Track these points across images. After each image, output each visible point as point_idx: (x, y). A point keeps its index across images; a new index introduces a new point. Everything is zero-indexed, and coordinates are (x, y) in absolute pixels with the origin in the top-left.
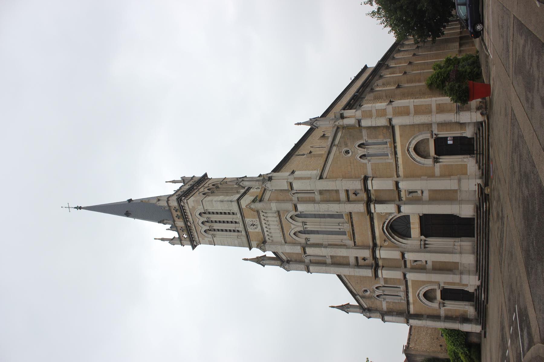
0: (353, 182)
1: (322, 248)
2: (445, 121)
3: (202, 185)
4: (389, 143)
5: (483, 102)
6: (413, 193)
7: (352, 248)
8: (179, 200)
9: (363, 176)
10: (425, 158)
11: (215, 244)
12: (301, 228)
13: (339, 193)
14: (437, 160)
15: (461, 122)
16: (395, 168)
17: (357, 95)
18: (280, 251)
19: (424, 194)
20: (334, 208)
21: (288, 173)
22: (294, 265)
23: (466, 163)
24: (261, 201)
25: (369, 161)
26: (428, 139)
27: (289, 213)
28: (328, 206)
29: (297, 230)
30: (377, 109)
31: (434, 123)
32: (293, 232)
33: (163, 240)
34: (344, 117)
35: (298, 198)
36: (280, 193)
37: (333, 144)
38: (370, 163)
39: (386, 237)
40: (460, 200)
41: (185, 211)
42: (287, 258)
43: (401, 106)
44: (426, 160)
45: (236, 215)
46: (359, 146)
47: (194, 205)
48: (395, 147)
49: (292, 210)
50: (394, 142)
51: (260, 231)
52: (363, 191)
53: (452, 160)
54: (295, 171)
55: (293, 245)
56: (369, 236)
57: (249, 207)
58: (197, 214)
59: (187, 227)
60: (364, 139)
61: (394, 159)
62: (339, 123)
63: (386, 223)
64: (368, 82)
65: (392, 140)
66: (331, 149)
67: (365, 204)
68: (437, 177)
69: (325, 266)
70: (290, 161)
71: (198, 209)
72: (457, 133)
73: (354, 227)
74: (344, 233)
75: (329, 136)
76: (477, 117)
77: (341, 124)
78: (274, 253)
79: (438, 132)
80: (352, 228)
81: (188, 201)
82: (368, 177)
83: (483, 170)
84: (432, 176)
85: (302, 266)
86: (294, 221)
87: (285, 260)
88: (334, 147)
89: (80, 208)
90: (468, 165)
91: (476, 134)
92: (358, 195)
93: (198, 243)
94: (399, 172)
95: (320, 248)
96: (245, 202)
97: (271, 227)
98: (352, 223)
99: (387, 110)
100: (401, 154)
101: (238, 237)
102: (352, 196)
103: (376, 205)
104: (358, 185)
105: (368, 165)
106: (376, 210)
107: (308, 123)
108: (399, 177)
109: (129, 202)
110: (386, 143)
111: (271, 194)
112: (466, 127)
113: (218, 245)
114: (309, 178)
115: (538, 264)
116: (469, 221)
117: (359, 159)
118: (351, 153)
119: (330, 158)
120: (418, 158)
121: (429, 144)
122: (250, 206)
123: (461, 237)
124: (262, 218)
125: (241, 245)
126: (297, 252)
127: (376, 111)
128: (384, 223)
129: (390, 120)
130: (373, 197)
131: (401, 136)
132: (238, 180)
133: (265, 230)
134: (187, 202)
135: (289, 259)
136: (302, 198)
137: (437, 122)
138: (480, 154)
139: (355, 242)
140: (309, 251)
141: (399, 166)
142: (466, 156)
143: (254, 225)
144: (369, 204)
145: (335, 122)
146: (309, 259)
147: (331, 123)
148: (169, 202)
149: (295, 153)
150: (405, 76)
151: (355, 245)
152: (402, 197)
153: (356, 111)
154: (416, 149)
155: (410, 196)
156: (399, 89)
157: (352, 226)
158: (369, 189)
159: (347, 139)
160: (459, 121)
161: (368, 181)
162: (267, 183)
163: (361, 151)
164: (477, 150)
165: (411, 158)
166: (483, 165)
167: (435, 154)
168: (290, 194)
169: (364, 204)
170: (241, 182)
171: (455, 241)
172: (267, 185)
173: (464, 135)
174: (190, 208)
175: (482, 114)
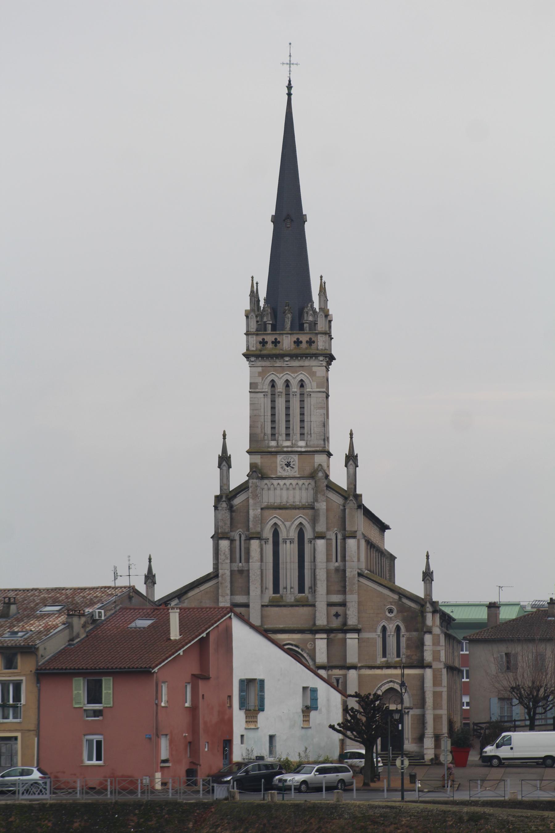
0: (355, 616)
2: (426, 723)
4: (399, 660)
12: (286, 535)
20: (321, 588)
25: (379, 636)
27: (308, 523)
28: (324, 580)
32: (279, 523)
37: (402, 596)
38: (377, 636)
42: (236, 505)
45: (299, 439)
51: (279, 474)
62: (428, 607)
63: (297, 649)
71: (311, 380)
73: (290, 608)
76: (429, 754)
80: (288, 605)
89: (289, 95)
92: (334, 618)
94: (364, 670)
102: (334, 610)
103: (326, 641)
110: (398, 655)
111: (336, 502)
117: (382, 625)
118: (389, 615)
122: (320, 470)
124: (301, 482)
128: (296, 646)
129: (430, 667)
130: (332, 635)
133: (282, 482)
136: (331, 544)
139: (267, 606)
152: (332, 671)
157: (292, 606)
162: (355, 503)
165: (381, 684)
172: (351, 502)
173: (406, 742)
174: (313, 368)
175: (432, 760)
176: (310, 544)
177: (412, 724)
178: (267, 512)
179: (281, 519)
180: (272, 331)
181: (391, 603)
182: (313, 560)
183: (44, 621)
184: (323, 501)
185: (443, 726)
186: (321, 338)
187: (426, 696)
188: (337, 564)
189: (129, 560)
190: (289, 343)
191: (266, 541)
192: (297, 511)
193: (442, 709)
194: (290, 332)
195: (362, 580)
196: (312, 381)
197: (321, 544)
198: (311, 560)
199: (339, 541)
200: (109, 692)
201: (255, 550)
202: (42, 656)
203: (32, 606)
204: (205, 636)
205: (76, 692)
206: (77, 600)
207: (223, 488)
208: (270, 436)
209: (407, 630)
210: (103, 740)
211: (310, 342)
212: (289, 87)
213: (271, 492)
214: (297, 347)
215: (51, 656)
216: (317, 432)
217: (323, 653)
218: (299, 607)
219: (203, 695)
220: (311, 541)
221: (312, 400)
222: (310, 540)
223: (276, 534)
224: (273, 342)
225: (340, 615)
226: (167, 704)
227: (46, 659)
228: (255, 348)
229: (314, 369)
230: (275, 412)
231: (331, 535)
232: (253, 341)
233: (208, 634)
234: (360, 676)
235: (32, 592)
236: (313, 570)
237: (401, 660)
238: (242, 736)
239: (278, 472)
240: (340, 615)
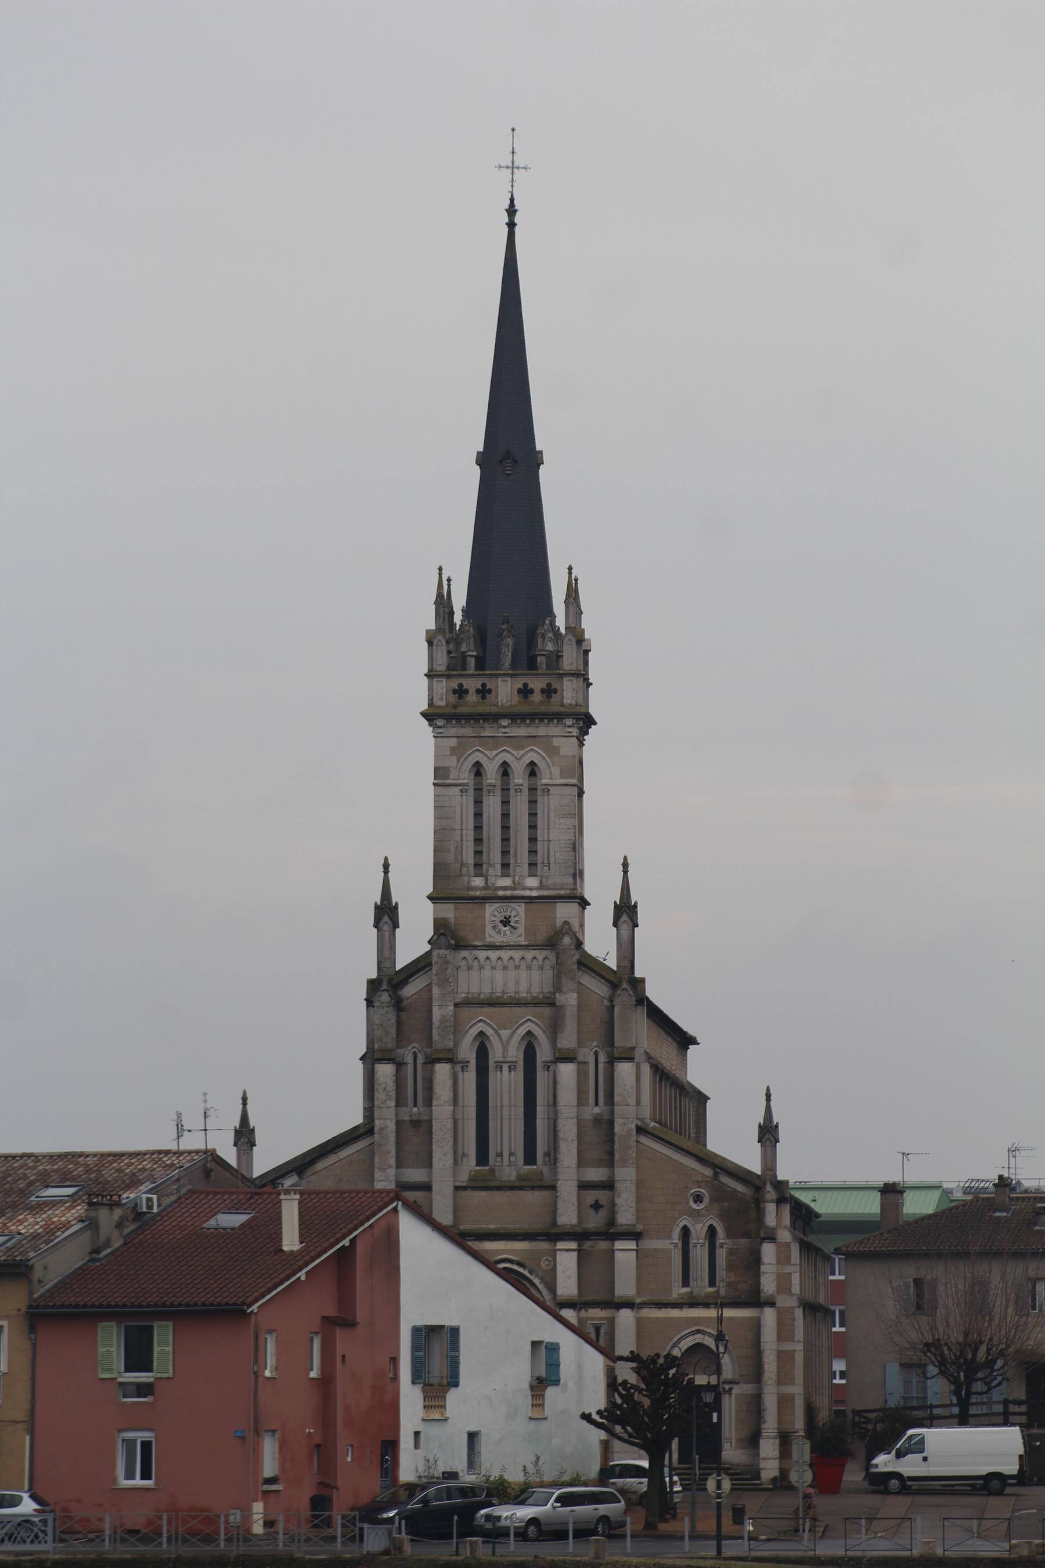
0: (631, 1207)
2: (764, 1410)
11: (437, 787)
12: (501, 1056)
13: (597, 1167)
27: (544, 1032)
28: (573, 1141)
31: (397, 1114)
32: (489, 1032)
38: (672, 1247)
42: (407, 998)
45: (527, 875)
49: (559, 1045)
62: (769, 1192)
63: (521, 1270)
73: (509, 1193)
75: (904, 1282)
89: (511, 225)
92: (592, 1211)
94: (648, 1309)
102: (591, 1196)
103: (575, 1254)
105: (667, 1242)
106: (564, 1252)
110: (712, 1283)
112: (743, 1449)
115: (980, 1377)
117: (681, 1225)
118: (695, 1206)
122: (566, 933)
124: (529, 955)
127: (787, 1273)
129: (772, 1304)
130: (587, 1245)
133: (493, 955)
135: (406, 1002)
139: (465, 1188)
147: (768, 1172)
152: (587, 1311)
157: (511, 1188)
162: (632, 994)
163: (698, 1230)
165: (679, 1336)
173: (726, 1446)
174: (554, 739)
175: (774, 1480)
176: (546, 1072)
177: (737, 1412)
178: (465, 1012)
179: (491, 1023)
180: (476, 669)
181: (699, 1184)
182: (551, 1102)
183: (44, 1216)
184: (572, 991)
185: (796, 1415)
189: (205, 1101)
191: (464, 1066)
193: (793, 1384)
194: (511, 672)
195: (644, 1140)
196: (551, 765)
197: (567, 1071)
198: (548, 1101)
199: (601, 1066)
200: (166, 1349)
201: (444, 1082)
202: (40, 1282)
203: (21, 1186)
204: (347, 1244)
205: (104, 1349)
206: (106, 1176)
209: (730, 1235)
210: (153, 1440)
211: (549, 691)
212: (512, 211)
214: (523, 700)
215: (55, 1281)
216: (560, 861)
217: (570, 1277)
219: (344, 1356)
220: (549, 1067)
221: (551, 801)
222: (547, 1064)
224: (478, 691)
225: (602, 1206)
226: (275, 1373)
227: (47, 1287)
229: (556, 742)
230: (482, 823)
231: (586, 1055)
232: (442, 689)
233: (353, 1241)
235: (21, 1161)
236: (552, 1121)
237: (718, 1292)
238: (417, 1434)
239: (487, 935)
240: (602, 1206)
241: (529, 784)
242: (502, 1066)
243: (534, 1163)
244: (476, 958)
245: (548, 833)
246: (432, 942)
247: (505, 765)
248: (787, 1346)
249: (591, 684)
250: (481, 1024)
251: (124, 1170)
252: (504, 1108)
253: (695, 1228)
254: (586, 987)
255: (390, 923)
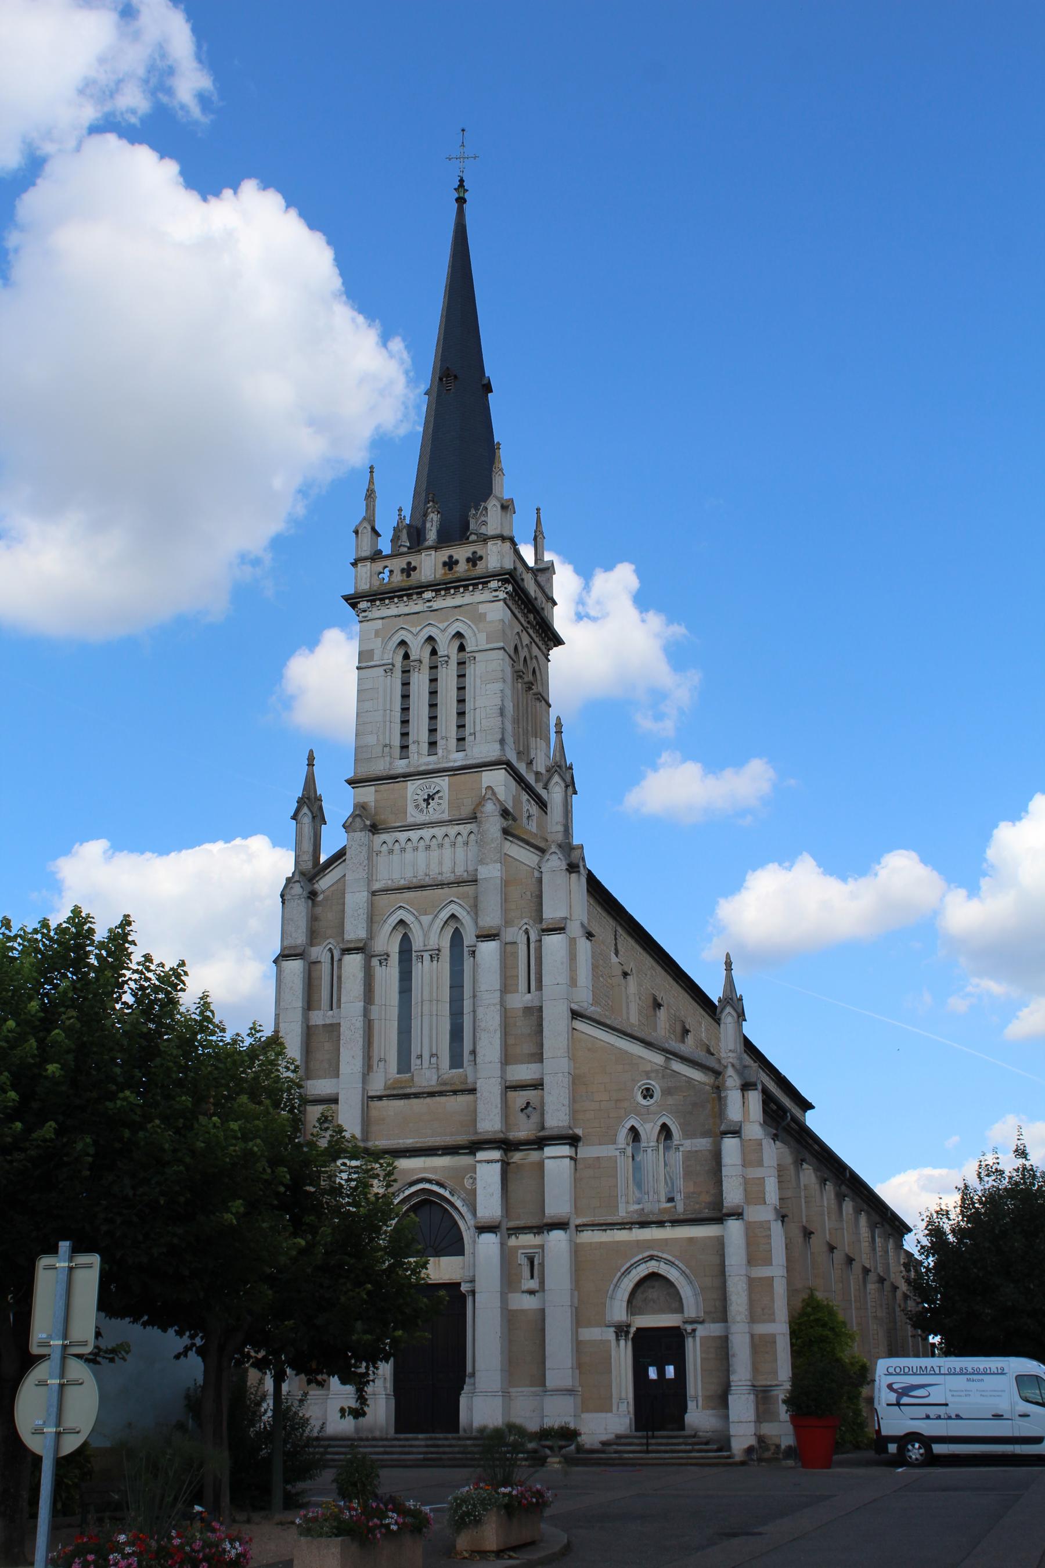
1: (362, 1004)
2: (733, 1356)
3: (537, 640)
4: (671, 1207)
5: (777, 1454)
6: (529, 1267)
7: (364, 1089)
8: (510, 577)
9: (579, 1132)
10: (630, 1301)
11: (361, 671)
12: (422, 944)
14: (623, 1334)
15: (730, 1398)
16: (602, 1222)
17: (787, 1117)
18: (352, 871)
19: (527, 1298)
20: (490, 1048)
21: (586, 922)
22: (304, 914)
23: (614, 1408)
24: (506, 832)
25: (623, 1152)
26: (680, 1309)
27: (468, 913)
28: (495, 1031)
29: (414, 930)
30: (766, 1182)
31: (727, 1328)
32: (409, 919)
33: (370, 495)
34: (745, 1093)
35: (515, 943)
36: (528, 893)
37: (671, 1057)
38: (617, 1153)
39: (399, 1190)
40: (511, 1394)
41: (471, 588)
43: (771, 1243)
44: (625, 1304)
46: (665, 1127)
47: (490, 622)
48: (661, 1224)
49: (481, 923)
50: (676, 1222)
51: (410, 820)
52: (540, 1131)
53: (623, 1372)
54: (591, 940)
55: (367, 918)
56: (401, 1141)
57: (487, 796)
58: (458, 627)
59: (417, 588)
60: (683, 1142)
61: (628, 1220)
63: (441, 1191)
64: (807, 1142)
65: (682, 1217)
66: (659, 1050)
67: (502, 1136)
68: (577, 1333)
69: (303, 1008)
70: (604, 914)
71: (476, 630)
72: (696, 1386)
73: (428, 1100)
74: (404, 1064)
76: (743, 1435)
77: (727, 1083)
78: (340, 856)
79: (701, 1338)
80: (423, 1093)
81: (502, 603)
82: (576, 1147)
83: (603, 1452)
84: (579, 1320)
85: (300, 938)
86: (441, 925)
87: (316, 886)
88: (664, 1058)
89: (461, 201)
90: (609, 1415)
91: (694, 1436)
92: (522, 1117)
93: (364, 614)
94: (590, 1232)
95: (362, 996)
96: (497, 779)
97: (421, 855)
98: (441, 1093)
99: (760, 1208)
100: (641, 1238)
101: (386, 746)
102: (519, 1098)
103: (498, 1165)
104: (556, 1119)
106: (484, 1164)
107: (731, 991)
108: (577, 1230)
109: (484, 385)
113: (360, 680)
114: (573, 982)
116: (449, 1418)
117: (628, 1126)
118: (644, 1102)
119: (632, 1044)
120: (628, 1284)
121: (665, 1314)
123: (394, 1395)
124: (452, 830)
125: (361, 753)
126: (348, 927)
127: (759, 1179)
129: (738, 1215)
130: (517, 1157)
131: (691, 1240)
132: (566, 770)
133: (414, 835)
134: (499, 600)
136: (515, 955)
137: (730, 1336)
138: (647, 1444)
139: (380, 1098)
140: (353, 963)
141: (608, 1231)
142: (632, 1409)
143: (429, 804)
144: (503, 1146)
145: (733, 1065)
146: (322, 961)
147: (730, 1054)
148: (499, 542)
149: (621, 925)
150: (825, 1248)
151: (372, 1097)
152: (517, 1238)
153: (761, 1124)
154: (653, 1276)
155: (523, 1261)
156: (801, 1235)
157: (432, 1094)
158: (546, 1149)
159: (684, 1096)
160: (732, 1392)
161: (567, 1147)
162: (562, 858)
163: (649, 1131)
164: (653, 1437)
165: (628, 1265)
166: (616, 1452)
167: (638, 1329)
168: (525, 920)
169: (502, 1132)
170: (564, 780)
171: (385, 1379)
172: (554, 857)
173: (691, 1405)
174: (480, 606)
175: (750, 1450)
177: (702, 1359)
178: (382, 900)
179: (411, 909)
181: (647, 1075)
184: (495, 862)
185: (779, 1362)
186: (494, 549)
187: (731, 1289)
188: (529, 996)
190: (433, 565)
192: (446, 890)
193: (774, 1321)
195: (579, 1025)
196: (477, 632)
197: (489, 950)
201: (354, 976)
207: (300, 860)
208: (398, 750)
211: (474, 560)
213: (395, 857)
214: (448, 572)
216: (486, 729)
218: (446, 1095)
221: (477, 668)
222: (471, 949)
223: (406, 942)
228: (368, 584)
229: (482, 608)
231: (514, 934)
232: (366, 573)
234: (576, 1250)
237: (675, 1207)
241: (458, 659)
242: (422, 956)
243: (461, 1066)
244: (397, 841)
245: (474, 702)
246: (347, 825)
247: (430, 639)
248: (754, 1173)
249: (467, 190)
250: (401, 911)
251: (385, 1254)
252: (424, 1003)
253: (645, 1129)
254: (514, 858)
255: (309, 814)
